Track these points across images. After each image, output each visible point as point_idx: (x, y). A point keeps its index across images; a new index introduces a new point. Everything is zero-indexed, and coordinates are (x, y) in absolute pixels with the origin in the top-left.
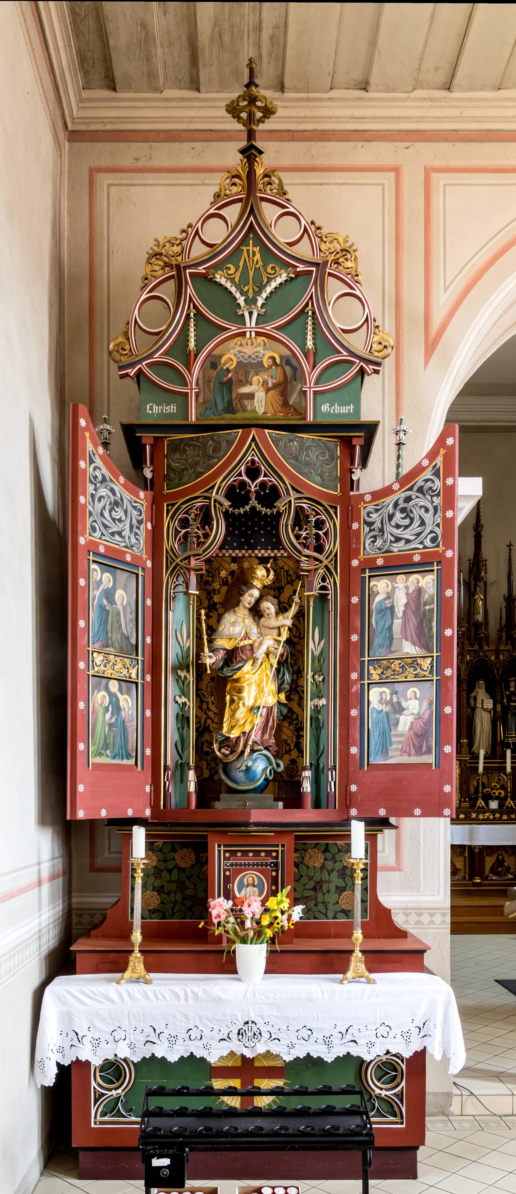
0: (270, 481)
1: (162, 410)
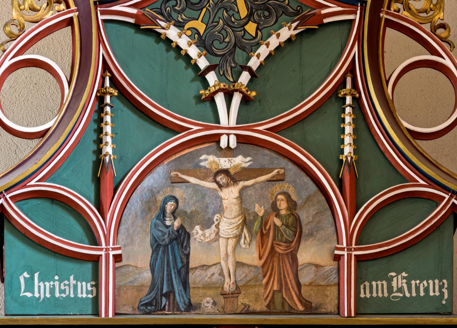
1: (52, 291)
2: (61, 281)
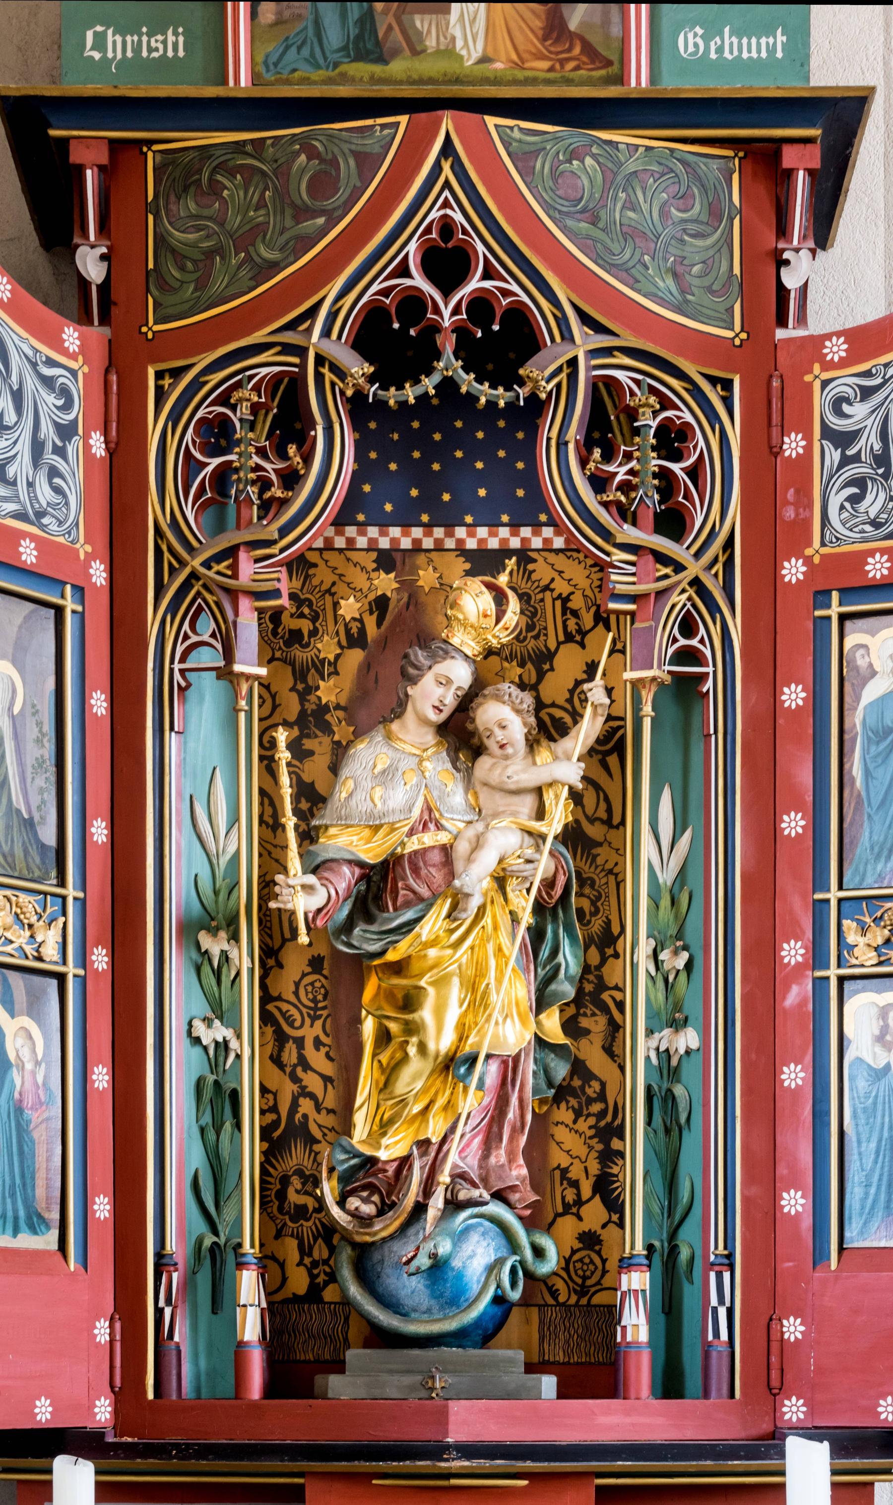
0: (506, 293)
1: (137, 49)
2: (150, 35)
